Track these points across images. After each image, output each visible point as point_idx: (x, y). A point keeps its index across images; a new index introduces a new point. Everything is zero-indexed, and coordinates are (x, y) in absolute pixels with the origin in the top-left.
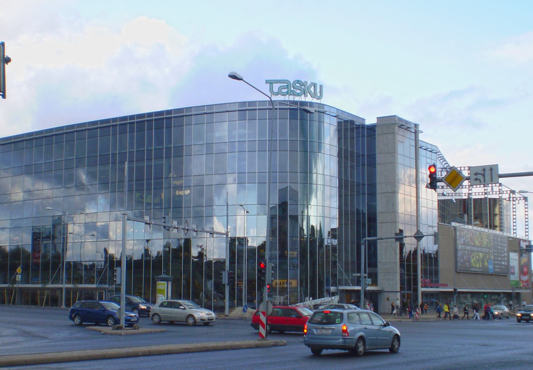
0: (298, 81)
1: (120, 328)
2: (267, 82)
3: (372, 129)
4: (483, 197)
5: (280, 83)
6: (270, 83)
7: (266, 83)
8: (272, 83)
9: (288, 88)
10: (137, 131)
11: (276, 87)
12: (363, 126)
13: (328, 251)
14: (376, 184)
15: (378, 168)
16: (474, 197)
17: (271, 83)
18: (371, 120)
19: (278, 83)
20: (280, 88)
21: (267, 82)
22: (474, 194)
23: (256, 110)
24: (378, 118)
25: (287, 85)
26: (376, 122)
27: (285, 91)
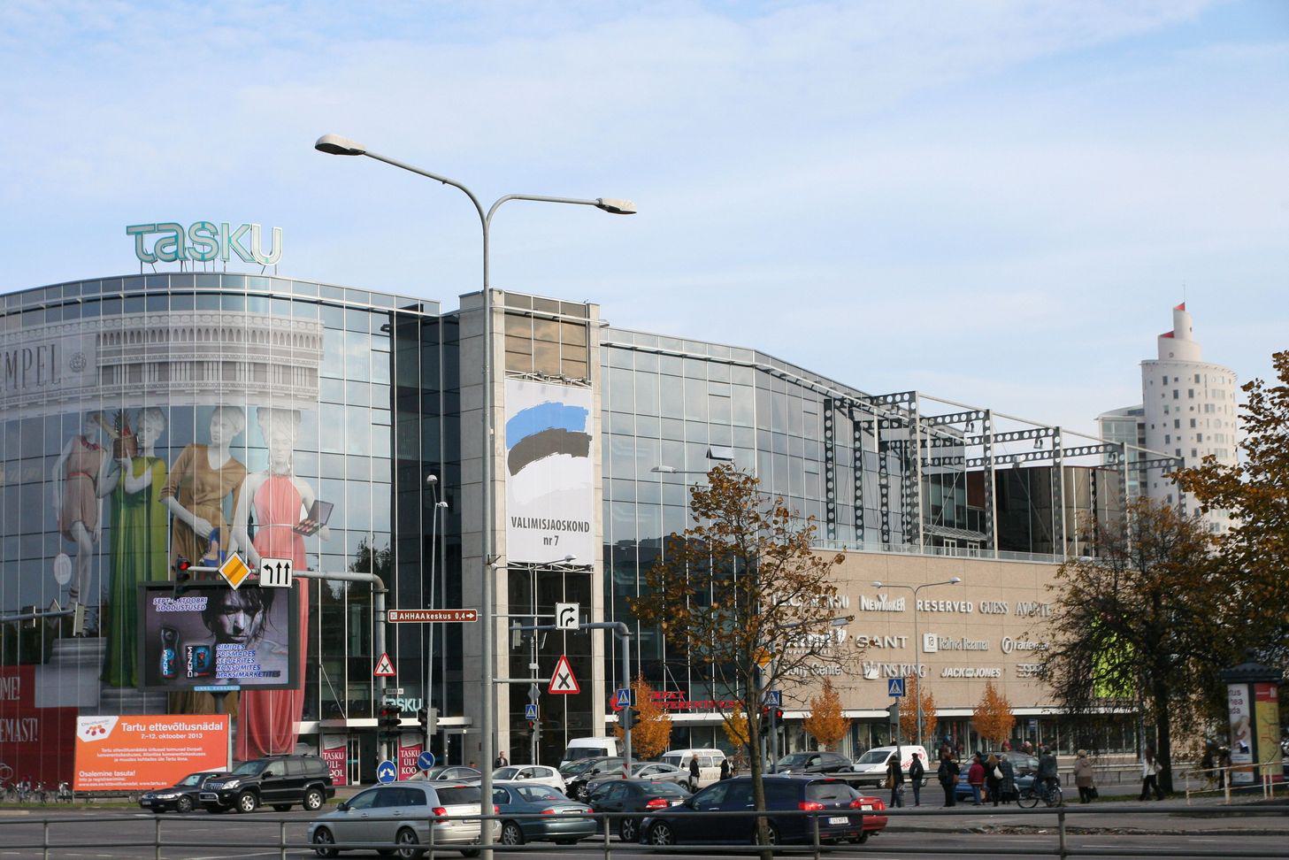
0: (203, 223)
1: (100, 727)
2: (129, 230)
3: (451, 321)
4: (1049, 463)
5: (159, 231)
6: (137, 234)
7: (128, 233)
8: (141, 233)
9: (177, 241)
10: (444, 343)
11: (150, 242)
12: (430, 322)
13: (129, 672)
14: (460, 461)
15: (463, 417)
16: (995, 467)
17: (137, 232)
18: (449, 305)
19: (153, 232)
20: (161, 245)
21: (129, 230)
22: (994, 461)
23: (142, 295)
24: (461, 297)
25: (176, 237)
26: (458, 308)
27: (170, 249)
